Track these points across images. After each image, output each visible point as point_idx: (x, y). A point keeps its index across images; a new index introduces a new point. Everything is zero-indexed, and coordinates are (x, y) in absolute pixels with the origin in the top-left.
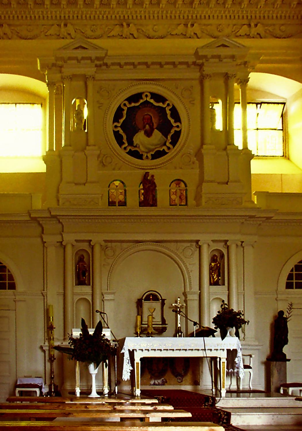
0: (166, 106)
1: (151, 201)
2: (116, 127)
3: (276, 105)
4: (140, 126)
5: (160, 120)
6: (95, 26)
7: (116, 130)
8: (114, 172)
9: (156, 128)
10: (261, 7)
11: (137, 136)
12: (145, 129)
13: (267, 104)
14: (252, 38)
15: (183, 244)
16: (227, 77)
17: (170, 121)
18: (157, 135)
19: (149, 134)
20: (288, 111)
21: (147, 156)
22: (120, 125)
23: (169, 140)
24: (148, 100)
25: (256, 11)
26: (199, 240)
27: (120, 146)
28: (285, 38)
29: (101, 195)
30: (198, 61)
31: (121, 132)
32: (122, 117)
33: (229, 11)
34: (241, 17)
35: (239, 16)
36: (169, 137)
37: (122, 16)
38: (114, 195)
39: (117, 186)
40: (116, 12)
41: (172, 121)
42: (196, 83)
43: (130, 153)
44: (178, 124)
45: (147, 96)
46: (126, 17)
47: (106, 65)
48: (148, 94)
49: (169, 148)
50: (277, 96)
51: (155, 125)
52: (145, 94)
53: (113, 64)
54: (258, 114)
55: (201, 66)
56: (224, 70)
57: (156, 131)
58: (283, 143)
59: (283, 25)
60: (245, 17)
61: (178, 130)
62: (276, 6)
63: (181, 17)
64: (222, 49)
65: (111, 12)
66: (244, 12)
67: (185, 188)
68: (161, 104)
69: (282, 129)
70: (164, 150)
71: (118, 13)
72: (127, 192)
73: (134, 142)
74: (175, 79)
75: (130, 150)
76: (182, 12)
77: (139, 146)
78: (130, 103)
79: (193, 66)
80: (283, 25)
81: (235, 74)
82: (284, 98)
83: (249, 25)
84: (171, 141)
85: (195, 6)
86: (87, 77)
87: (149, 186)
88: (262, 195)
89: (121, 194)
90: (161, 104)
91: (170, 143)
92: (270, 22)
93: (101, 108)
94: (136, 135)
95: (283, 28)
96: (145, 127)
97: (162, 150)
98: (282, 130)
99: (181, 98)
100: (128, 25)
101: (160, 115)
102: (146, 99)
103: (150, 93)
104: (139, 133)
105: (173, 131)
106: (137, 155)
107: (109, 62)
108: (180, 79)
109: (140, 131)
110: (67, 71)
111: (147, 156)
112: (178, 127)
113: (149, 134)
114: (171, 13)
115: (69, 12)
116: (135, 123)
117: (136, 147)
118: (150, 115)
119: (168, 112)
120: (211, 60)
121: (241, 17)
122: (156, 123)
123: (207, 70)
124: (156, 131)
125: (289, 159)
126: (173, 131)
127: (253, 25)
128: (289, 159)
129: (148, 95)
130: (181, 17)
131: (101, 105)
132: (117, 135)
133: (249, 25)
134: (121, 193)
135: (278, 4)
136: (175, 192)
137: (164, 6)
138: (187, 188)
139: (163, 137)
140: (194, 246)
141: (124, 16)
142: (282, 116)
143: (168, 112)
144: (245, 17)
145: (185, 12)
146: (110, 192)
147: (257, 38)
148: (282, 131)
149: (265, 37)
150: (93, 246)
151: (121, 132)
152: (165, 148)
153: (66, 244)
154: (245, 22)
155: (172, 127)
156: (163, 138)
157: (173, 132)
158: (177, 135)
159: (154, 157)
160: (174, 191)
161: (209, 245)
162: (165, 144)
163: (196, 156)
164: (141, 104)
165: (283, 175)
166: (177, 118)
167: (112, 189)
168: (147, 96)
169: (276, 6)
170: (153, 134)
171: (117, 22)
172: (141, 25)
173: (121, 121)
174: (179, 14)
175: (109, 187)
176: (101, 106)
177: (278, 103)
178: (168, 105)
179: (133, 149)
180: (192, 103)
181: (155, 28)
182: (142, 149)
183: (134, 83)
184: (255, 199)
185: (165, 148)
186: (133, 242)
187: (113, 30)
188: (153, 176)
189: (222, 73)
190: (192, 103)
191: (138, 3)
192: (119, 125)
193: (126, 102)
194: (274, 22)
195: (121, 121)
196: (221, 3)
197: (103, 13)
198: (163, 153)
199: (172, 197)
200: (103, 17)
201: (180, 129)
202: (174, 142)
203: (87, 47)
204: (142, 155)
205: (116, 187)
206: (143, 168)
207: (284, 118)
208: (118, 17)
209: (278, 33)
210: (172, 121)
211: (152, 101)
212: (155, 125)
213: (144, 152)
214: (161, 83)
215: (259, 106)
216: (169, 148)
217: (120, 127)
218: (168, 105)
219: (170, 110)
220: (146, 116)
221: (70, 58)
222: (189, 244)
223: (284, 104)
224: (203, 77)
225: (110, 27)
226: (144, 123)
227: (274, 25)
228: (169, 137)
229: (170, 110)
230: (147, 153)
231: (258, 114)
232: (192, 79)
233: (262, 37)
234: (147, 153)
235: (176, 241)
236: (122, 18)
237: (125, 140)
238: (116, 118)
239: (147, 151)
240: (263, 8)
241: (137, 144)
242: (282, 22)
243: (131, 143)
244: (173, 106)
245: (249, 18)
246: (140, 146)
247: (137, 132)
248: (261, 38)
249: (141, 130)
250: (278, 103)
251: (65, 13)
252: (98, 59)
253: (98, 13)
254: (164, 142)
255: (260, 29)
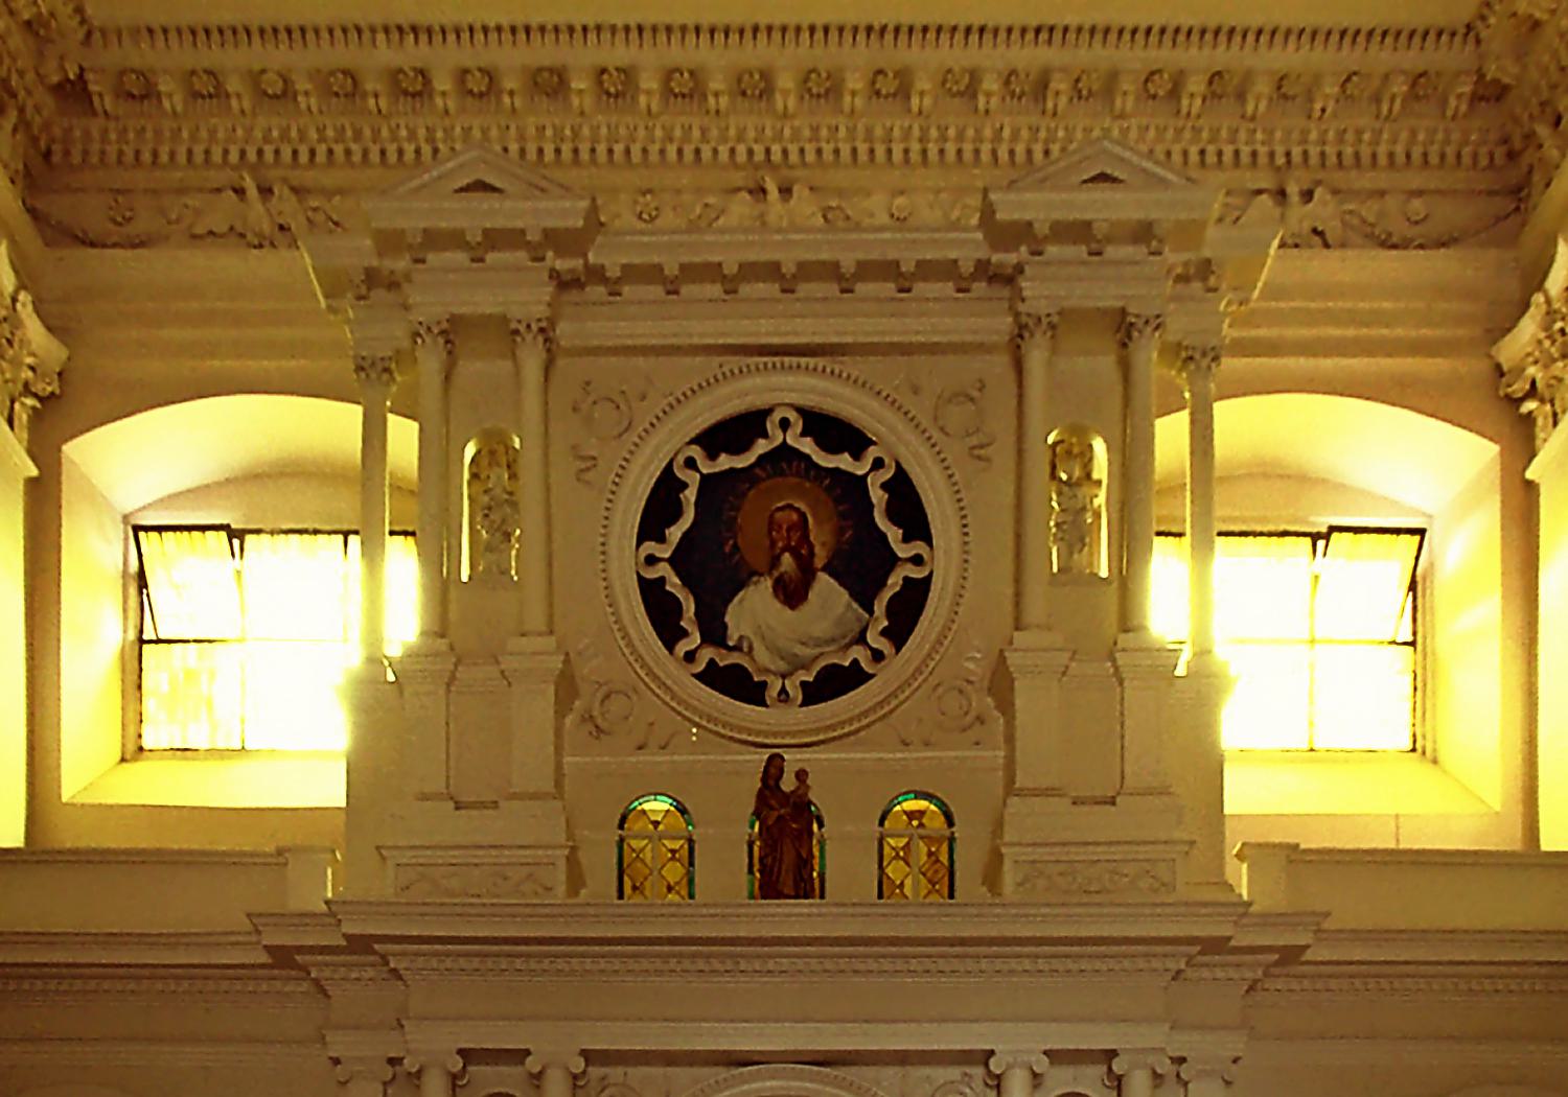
0: (867, 469)
1: (790, 882)
2: (651, 560)
3: (1387, 536)
4: (757, 558)
5: (840, 532)
6: (649, 197)
7: (651, 574)
8: (643, 757)
9: (824, 569)
10: (1323, 110)
11: (741, 601)
12: (776, 574)
13: (1351, 534)
14: (1290, 247)
15: (926, 1071)
16: (1123, 328)
17: (884, 536)
18: (828, 595)
19: (792, 593)
20: (1438, 564)
21: (783, 690)
22: (667, 555)
23: (877, 619)
24: (789, 441)
25: (1305, 133)
26: (992, 1053)
27: (670, 646)
28: (1421, 247)
29: (566, 852)
30: (995, 258)
31: (674, 584)
32: (676, 514)
33: (1197, 131)
34: (1245, 158)
35: (1237, 153)
36: (880, 607)
37: (759, 149)
38: (643, 861)
39: (656, 824)
40: (732, 132)
41: (893, 534)
42: (1001, 363)
43: (713, 677)
44: (919, 547)
45: (785, 424)
46: (776, 156)
47: (597, 274)
48: (792, 416)
49: (878, 656)
50: (1394, 503)
51: (820, 560)
52: (777, 416)
53: (631, 273)
54: (1316, 577)
55: (1008, 278)
56: (1107, 297)
57: (824, 580)
58: (1415, 696)
59: (1420, 193)
60: (1263, 159)
61: (917, 573)
62: (1385, 109)
63: (1003, 154)
64: (1101, 193)
65: (714, 133)
66: (1259, 136)
67: (947, 833)
68: (844, 462)
69: (1410, 639)
70: (855, 662)
71: (740, 138)
72: (696, 847)
73: (729, 632)
74: (906, 350)
75: (712, 662)
76: (1006, 133)
77: (751, 648)
78: (712, 456)
79: (980, 287)
80: (1420, 193)
81: (1158, 316)
82: (1424, 514)
83: (1281, 194)
84: (886, 623)
85: (1056, 106)
86: (514, 325)
87: (780, 818)
88: (1257, 853)
89: (673, 858)
90: (844, 462)
91: (884, 633)
92: (1366, 181)
93: (589, 476)
94: (736, 599)
95: (1417, 206)
96: (775, 561)
97: (847, 664)
98: (1413, 644)
99: (937, 436)
100: (786, 191)
101: (841, 508)
102: (780, 439)
103: (800, 410)
104: (752, 588)
105: (895, 582)
106: (739, 684)
107: (613, 263)
108: (933, 349)
109: (755, 579)
110: (430, 302)
111: (783, 690)
112: (917, 560)
113: (792, 593)
114: (960, 137)
115: (541, 129)
116: (735, 546)
117: (737, 648)
118: (797, 510)
119: (878, 496)
120: (1052, 250)
121: (1245, 158)
122: (823, 544)
123: (1038, 293)
124: (824, 580)
125: (1435, 761)
126: (895, 582)
127: (1293, 190)
128: (1435, 761)
129: (792, 420)
130: (1003, 154)
131: (589, 464)
132: (653, 594)
133: (1281, 194)
134: (673, 852)
135: (1393, 99)
136: (903, 848)
137: (927, 101)
138: (954, 829)
139: (855, 606)
140: (978, 1084)
141: (768, 151)
142: (1413, 587)
143: (878, 496)
144: (1263, 159)
145: (1015, 136)
146: (625, 847)
147: (1310, 246)
148: (1412, 648)
149: (1343, 245)
150: (1119, 1078)
151: (674, 584)
152: (858, 653)
153: (1010, 1067)
154: (1265, 180)
155: (893, 561)
156: (856, 610)
157: (895, 584)
158: (915, 595)
159: (814, 694)
160: (903, 842)
161: (1035, 1075)
162: (861, 639)
163: (990, 691)
164: (761, 458)
165: (1401, 820)
166: (916, 525)
167: (636, 837)
168: (785, 424)
169: (1385, 109)
170: (811, 595)
171: (738, 178)
172: (841, 193)
173: (675, 533)
174: (992, 141)
175: (621, 826)
176: (588, 469)
177: (1397, 531)
178: (878, 464)
179: (725, 660)
180: (979, 458)
181: (897, 207)
182: (762, 661)
183: (733, 362)
184: (1241, 879)
185: (858, 653)
186: (716, 1064)
187: (723, 211)
188: (801, 775)
189: (1104, 312)
190: (979, 458)
191: (822, 91)
192: (665, 552)
193: (696, 452)
194: (1380, 179)
195: (675, 533)
196: (1161, 93)
197: (678, 133)
198: (852, 677)
199: (889, 871)
200: (680, 152)
201: (926, 573)
202: (900, 628)
203: (498, 184)
204: (764, 685)
205: (651, 827)
206: (759, 740)
207: (1419, 594)
208: (741, 156)
209: (1401, 229)
210: (893, 534)
211: (807, 446)
212: (820, 560)
213: (768, 671)
214: (851, 366)
215: (1321, 544)
216: (878, 656)
217: (670, 561)
218: (878, 464)
219: (884, 486)
220: (779, 515)
221: (434, 240)
222: (954, 1073)
223: (1421, 532)
224: (1022, 327)
225: (711, 200)
226: (773, 543)
227: (1382, 193)
228: (880, 606)
229: (884, 486)
230: (784, 677)
231: (1316, 577)
232: (981, 348)
233: (1330, 241)
234: (784, 677)
235: (903, 1058)
236: (759, 156)
237: (688, 620)
238: (653, 524)
239: (782, 666)
240: (1335, 115)
241: (741, 638)
242: (1415, 180)
243: (714, 632)
244: (899, 468)
245: (1280, 160)
246: (755, 645)
247: (741, 585)
248: (1327, 245)
249: (761, 575)
250: (1397, 531)
251: (522, 138)
252: (554, 239)
253: (659, 133)
254: (857, 629)
255: (1323, 210)
